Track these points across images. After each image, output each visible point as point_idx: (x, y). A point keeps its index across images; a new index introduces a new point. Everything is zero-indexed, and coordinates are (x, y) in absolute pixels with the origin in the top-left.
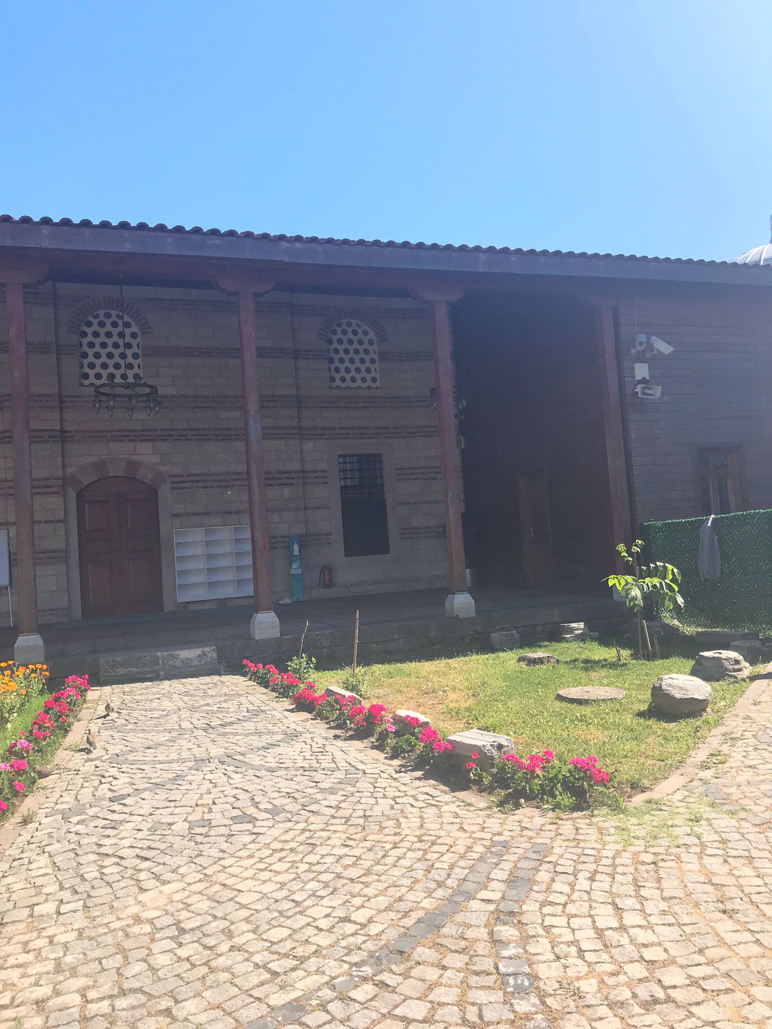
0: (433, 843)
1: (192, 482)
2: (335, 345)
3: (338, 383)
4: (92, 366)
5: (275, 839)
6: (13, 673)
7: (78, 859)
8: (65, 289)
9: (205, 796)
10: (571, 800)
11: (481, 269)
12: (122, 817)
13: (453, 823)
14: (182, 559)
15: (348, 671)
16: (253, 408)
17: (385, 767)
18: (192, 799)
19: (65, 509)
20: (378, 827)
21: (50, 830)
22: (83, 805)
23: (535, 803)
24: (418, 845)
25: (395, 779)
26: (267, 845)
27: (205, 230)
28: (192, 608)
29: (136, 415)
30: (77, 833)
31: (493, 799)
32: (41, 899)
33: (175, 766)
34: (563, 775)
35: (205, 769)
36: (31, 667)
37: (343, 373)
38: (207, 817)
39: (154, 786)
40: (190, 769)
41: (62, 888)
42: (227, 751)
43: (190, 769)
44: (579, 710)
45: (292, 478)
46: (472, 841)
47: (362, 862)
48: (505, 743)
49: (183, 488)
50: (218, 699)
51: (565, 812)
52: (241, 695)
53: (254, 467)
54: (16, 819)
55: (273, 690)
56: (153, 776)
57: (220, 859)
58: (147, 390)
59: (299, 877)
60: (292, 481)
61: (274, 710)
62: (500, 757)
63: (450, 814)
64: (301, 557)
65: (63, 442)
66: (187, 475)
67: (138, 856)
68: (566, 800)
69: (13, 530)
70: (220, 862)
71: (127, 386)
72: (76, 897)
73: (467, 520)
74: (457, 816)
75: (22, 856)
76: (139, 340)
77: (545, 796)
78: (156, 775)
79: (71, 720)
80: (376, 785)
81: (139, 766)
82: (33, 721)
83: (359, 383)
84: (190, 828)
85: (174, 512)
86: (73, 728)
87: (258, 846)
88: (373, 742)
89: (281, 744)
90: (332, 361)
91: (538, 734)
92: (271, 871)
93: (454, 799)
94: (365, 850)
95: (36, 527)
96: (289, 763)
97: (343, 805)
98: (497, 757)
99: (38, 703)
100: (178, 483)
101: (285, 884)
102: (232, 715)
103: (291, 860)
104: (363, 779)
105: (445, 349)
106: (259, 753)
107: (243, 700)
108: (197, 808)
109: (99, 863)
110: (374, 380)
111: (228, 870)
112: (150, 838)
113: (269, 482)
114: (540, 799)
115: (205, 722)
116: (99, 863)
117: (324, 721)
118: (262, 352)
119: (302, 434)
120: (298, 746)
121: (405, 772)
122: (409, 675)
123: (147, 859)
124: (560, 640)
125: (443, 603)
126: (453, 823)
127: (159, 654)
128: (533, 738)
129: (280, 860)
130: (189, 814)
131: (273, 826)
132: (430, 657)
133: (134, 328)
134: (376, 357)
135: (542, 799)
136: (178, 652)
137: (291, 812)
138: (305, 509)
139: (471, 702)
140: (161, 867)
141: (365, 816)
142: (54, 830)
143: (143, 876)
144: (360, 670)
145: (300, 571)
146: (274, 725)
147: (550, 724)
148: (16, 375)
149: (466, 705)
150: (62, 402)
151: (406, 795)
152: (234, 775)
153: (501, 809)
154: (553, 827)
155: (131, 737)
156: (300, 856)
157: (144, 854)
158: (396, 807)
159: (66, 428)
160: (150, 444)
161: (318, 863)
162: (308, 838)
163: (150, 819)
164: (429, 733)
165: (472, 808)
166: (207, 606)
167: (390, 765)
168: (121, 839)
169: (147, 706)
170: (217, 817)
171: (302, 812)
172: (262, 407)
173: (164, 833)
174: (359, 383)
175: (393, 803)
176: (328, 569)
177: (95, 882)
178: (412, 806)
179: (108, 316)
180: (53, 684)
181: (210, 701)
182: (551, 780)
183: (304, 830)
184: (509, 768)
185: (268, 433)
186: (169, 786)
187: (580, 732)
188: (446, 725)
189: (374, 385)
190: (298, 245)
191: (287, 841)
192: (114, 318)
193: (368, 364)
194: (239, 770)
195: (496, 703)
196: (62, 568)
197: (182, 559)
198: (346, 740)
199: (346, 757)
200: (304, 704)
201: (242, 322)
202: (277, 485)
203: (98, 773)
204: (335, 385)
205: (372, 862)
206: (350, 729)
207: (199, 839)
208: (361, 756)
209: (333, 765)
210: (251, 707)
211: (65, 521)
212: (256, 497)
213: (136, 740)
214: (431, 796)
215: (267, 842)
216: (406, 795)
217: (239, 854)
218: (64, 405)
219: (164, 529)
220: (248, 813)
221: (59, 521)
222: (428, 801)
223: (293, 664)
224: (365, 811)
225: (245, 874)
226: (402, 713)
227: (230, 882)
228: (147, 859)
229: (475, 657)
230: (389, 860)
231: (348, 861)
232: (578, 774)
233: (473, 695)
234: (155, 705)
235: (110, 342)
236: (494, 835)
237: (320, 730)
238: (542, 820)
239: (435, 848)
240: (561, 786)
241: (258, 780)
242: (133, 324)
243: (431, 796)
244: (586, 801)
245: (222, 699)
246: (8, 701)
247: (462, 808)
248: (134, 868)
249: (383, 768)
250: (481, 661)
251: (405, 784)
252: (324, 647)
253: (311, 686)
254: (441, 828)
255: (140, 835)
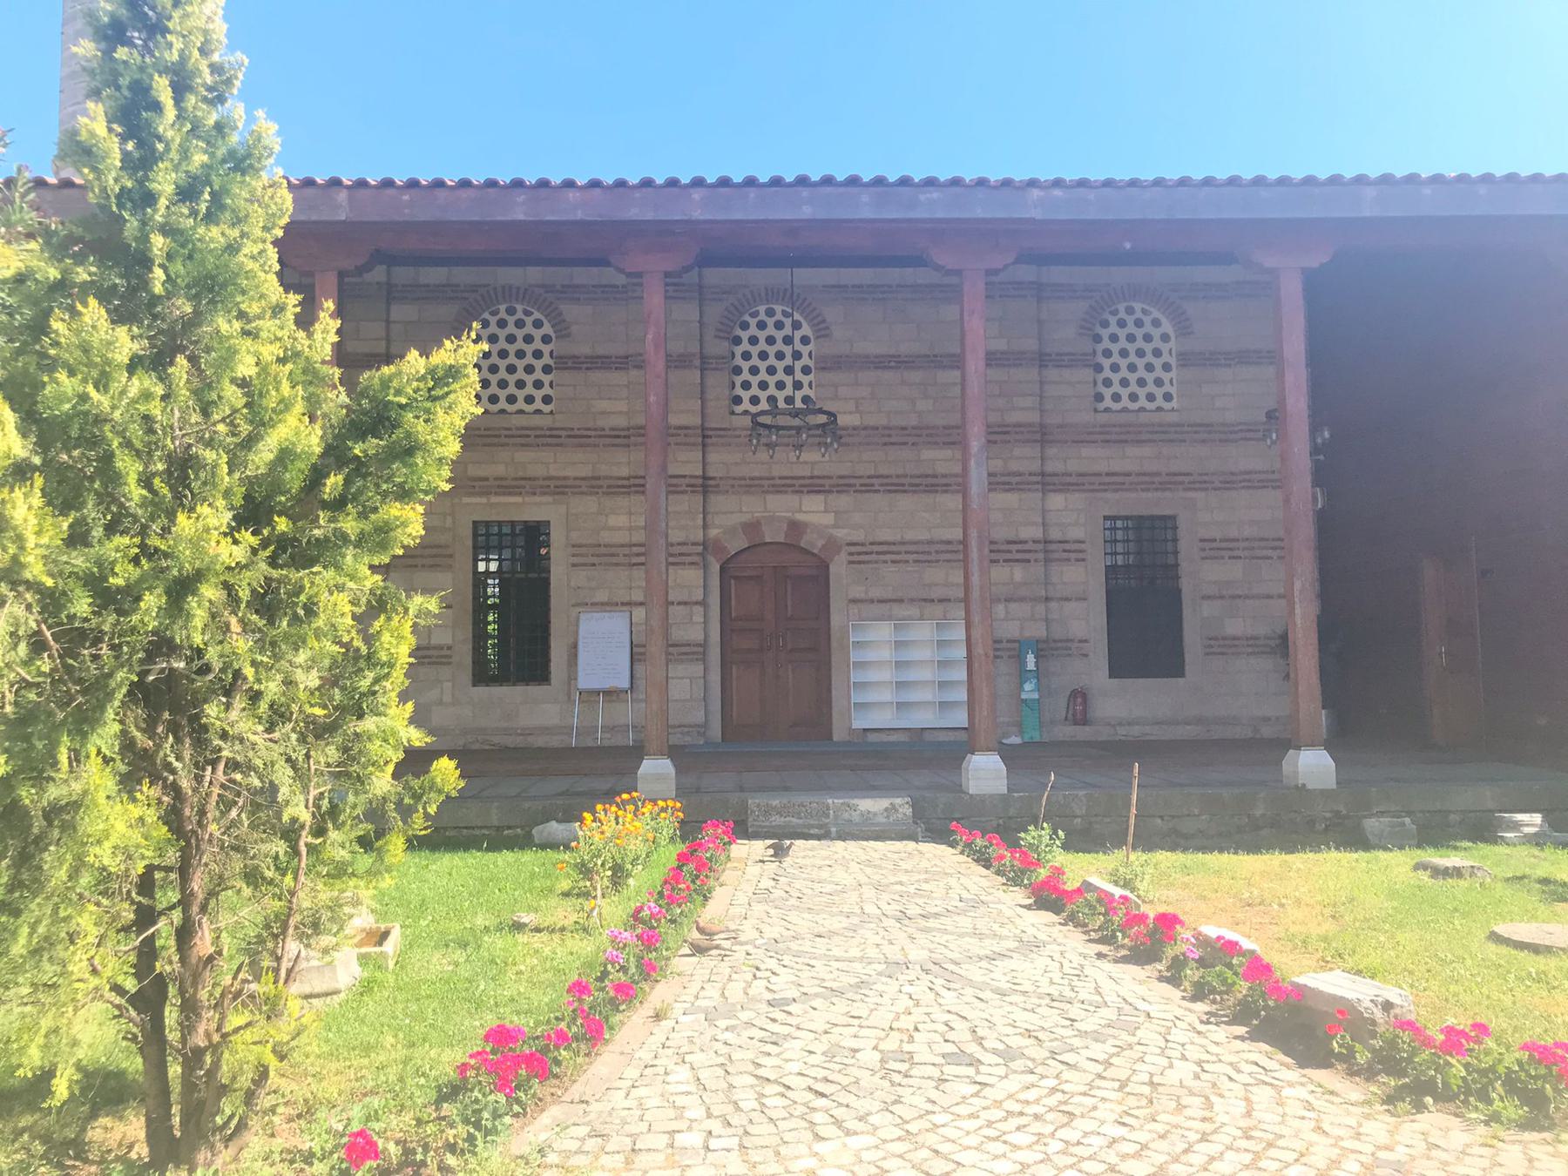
0: (1270, 1145)
1: (877, 553)
2: (1106, 343)
3: (1108, 403)
4: (746, 385)
5: (1010, 1096)
6: (637, 809)
7: (729, 1078)
8: (713, 276)
9: (902, 1016)
10: (1520, 1112)
11: (1367, 213)
12: (785, 1030)
13: (1303, 1118)
14: (861, 665)
15: (1119, 855)
16: (975, 445)
17: (1179, 1012)
18: (883, 1018)
19: (705, 587)
20: (1173, 1104)
21: (690, 1033)
22: (734, 1005)
23: (1452, 1106)
24: (1243, 1144)
25: (1199, 1033)
26: (998, 1104)
27: (917, 180)
28: (872, 737)
29: (805, 456)
30: (726, 1043)
31: (1374, 1088)
32: (682, 1125)
33: (857, 966)
34: (1507, 1068)
35: (901, 977)
36: (661, 803)
37: (1116, 388)
38: (907, 1047)
39: (829, 993)
40: (880, 974)
41: (709, 1116)
42: (933, 955)
43: (880, 974)
44: (1534, 963)
45: (1030, 551)
46: (1339, 1151)
47: (1149, 1153)
48: (1396, 1000)
49: (864, 562)
50: (917, 877)
51: (1509, 1129)
52: (951, 875)
53: (973, 533)
54: (646, 1010)
55: (998, 873)
56: (827, 977)
57: (928, 1112)
58: (822, 419)
59: (1050, 1160)
60: (1027, 556)
61: (1000, 902)
62: (1386, 1022)
63: (1298, 1102)
64: (1038, 673)
65: (705, 493)
66: (871, 544)
67: (810, 1089)
68: (1513, 1109)
69: (639, 614)
70: (928, 1117)
71: (796, 414)
72: (730, 1131)
73: (1328, 629)
74: (1309, 1106)
75: (655, 1062)
76: (810, 347)
77: (1471, 1099)
78: (832, 976)
79: (712, 882)
80: (1168, 1037)
81: (807, 961)
82: (662, 878)
83: (1143, 402)
84: (882, 1061)
85: (850, 597)
86: (714, 893)
87: (985, 1103)
88: (1160, 971)
89: (1014, 954)
90: (1098, 368)
91: (1456, 995)
92: (1005, 1142)
93: (1304, 1080)
94: (1155, 1136)
95: (671, 608)
96: (1027, 986)
97: (1114, 1060)
98: (1381, 1021)
99: (669, 855)
100: (859, 554)
101: (1029, 1166)
102: (938, 903)
103: (1037, 1131)
104: (1147, 1025)
105: (1295, 347)
106: (979, 964)
107: (953, 882)
108: (893, 1033)
109: (757, 1089)
110: (1168, 397)
111: (941, 1131)
112: (826, 1065)
113: (994, 556)
114: (1462, 1102)
115: (899, 908)
116: (757, 1089)
117: (1080, 929)
118: (992, 359)
119: (1046, 482)
120: (1041, 962)
121: (1217, 1024)
122: (1218, 873)
123: (823, 1095)
124: (1494, 840)
125: (1279, 763)
126: (1303, 1118)
127: (830, 801)
128: (1447, 1000)
129: (1018, 1129)
130: (880, 1039)
131: (1006, 1077)
132: (1254, 848)
133: (806, 330)
134: (1173, 361)
135: (1466, 1102)
136: (855, 801)
137: (1033, 1060)
138: (1047, 599)
139: (1329, 927)
140: (844, 1109)
141: (1151, 1083)
142: (696, 1034)
143: (818, 1117)
144: (1137, 857)
145: (1036, 696)
146: (1002, 925)
147: (1479, 980)
148: (652, 399)
149: (1322, 930)
150: (705, 437)
151: (1220, 1061)
152: (943, 992)
153: (1391, 1107)
154: (1485, 1151)
155: (793, 917)
156: (1050, 1128)
157: (820, 1087)
158: (1204, 1076)
159: (711, 473)
160: (821, 497)
161: (1079, 1143)
162: (1061, 1103)
163: (825, 1038)
164: (1258, 968)
165: (1337, 1100)
166: (893, 738)
167: (1190, 1010)
168: (787, 1061)
169: (815, 874)
170: (923, 1054)
171: (1050, 1062)
172: (989, 441)
173: (846, 1061)
174: (1143, 402)
175: (1198, 1069)
176: (1080, 697)
177: (754, 1114)
178: (1230, 1079)
179: (770, 313)
180: (688, 829)
181: (904, 878)
182: (1483, 1073)
183: (1054, 1090)
184: (1404, 1042)
185: (998, 483)
186: (849, 995)
187: (1536, 1000)
188: (1284, 960)
189: (1167, 406)
190: (1057, 192)
191: (1027, 1102)
192: (779, 316)
193: (1159, 372)
194: (952, 985)
195: (1374, 933)
196: (698, 669)
197: (861, 665)
198: (1116, 961)
199: (1117, 988)
200: (1050, 897)
201: (966, 314)
202: (1005, 561)
203: (750, 963)
204: (1101, 406)
205: (1167, 1158)
206: (1123, 946)
207: (897, 1078)
208: (1142, 990)
209: (1098, 998)
210: (965, 895)
211: (704, 603)
212: (975, 579)
213: (802, 922)
214: (1264, 1068)
215: (999, 1098)
216: (1220, 1061)
217: (956, 1109)
218: (709, 441)
219: (836, 620)
220: (968, 1051)
221: (697, 603)
222: (1258, 1076)
223: (1029, 837)
224: (1152, 1075)
225: (967, 1141)
226: (1211, 931)
227: (945, 1148)
228: (823, 1095)
229: (1334, 855)
230: (1197, 1159)
231: (1131, 1148)
232: (1536, 1069)
233: (1333, 917)
234: (825, 874)
235: (771, 350)
236: (1379, 1148)
237: (1074, 943)
238: (1466, 1138)
239: (1273, 1153)
240: (1503, 1085)
241: (982, 1005)
242: (805, 324)
243: (1264, 1068)
244: (1547, 1116)
245: (924, 876)
246: (632, 847)
247: (1319, 1095)
248: (805, 1105)
249: (1179, 1012)
250: (1344, 862)
251: (1217, 1044)
252: (1076, 817)
253: (1059, 871)
254: (1282, 1122)
255: (812, 1059)
